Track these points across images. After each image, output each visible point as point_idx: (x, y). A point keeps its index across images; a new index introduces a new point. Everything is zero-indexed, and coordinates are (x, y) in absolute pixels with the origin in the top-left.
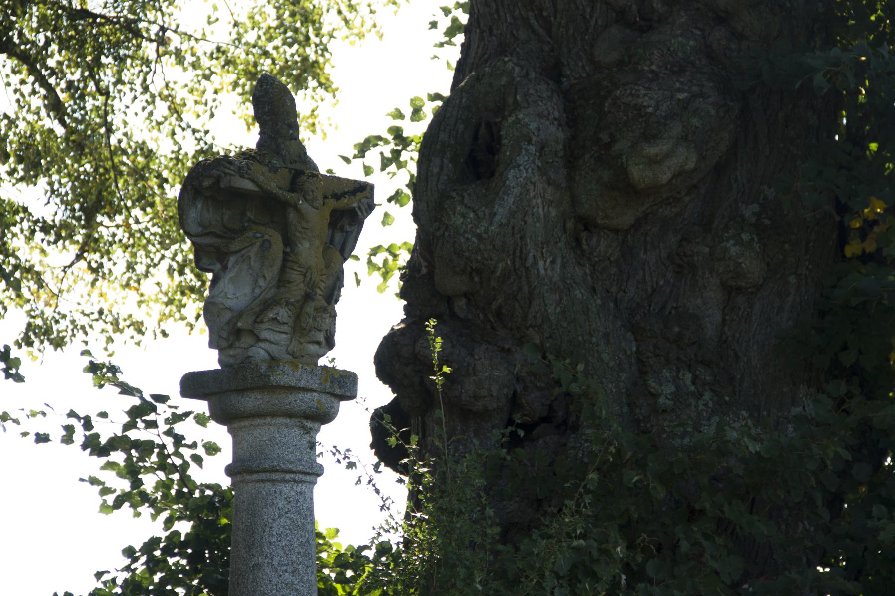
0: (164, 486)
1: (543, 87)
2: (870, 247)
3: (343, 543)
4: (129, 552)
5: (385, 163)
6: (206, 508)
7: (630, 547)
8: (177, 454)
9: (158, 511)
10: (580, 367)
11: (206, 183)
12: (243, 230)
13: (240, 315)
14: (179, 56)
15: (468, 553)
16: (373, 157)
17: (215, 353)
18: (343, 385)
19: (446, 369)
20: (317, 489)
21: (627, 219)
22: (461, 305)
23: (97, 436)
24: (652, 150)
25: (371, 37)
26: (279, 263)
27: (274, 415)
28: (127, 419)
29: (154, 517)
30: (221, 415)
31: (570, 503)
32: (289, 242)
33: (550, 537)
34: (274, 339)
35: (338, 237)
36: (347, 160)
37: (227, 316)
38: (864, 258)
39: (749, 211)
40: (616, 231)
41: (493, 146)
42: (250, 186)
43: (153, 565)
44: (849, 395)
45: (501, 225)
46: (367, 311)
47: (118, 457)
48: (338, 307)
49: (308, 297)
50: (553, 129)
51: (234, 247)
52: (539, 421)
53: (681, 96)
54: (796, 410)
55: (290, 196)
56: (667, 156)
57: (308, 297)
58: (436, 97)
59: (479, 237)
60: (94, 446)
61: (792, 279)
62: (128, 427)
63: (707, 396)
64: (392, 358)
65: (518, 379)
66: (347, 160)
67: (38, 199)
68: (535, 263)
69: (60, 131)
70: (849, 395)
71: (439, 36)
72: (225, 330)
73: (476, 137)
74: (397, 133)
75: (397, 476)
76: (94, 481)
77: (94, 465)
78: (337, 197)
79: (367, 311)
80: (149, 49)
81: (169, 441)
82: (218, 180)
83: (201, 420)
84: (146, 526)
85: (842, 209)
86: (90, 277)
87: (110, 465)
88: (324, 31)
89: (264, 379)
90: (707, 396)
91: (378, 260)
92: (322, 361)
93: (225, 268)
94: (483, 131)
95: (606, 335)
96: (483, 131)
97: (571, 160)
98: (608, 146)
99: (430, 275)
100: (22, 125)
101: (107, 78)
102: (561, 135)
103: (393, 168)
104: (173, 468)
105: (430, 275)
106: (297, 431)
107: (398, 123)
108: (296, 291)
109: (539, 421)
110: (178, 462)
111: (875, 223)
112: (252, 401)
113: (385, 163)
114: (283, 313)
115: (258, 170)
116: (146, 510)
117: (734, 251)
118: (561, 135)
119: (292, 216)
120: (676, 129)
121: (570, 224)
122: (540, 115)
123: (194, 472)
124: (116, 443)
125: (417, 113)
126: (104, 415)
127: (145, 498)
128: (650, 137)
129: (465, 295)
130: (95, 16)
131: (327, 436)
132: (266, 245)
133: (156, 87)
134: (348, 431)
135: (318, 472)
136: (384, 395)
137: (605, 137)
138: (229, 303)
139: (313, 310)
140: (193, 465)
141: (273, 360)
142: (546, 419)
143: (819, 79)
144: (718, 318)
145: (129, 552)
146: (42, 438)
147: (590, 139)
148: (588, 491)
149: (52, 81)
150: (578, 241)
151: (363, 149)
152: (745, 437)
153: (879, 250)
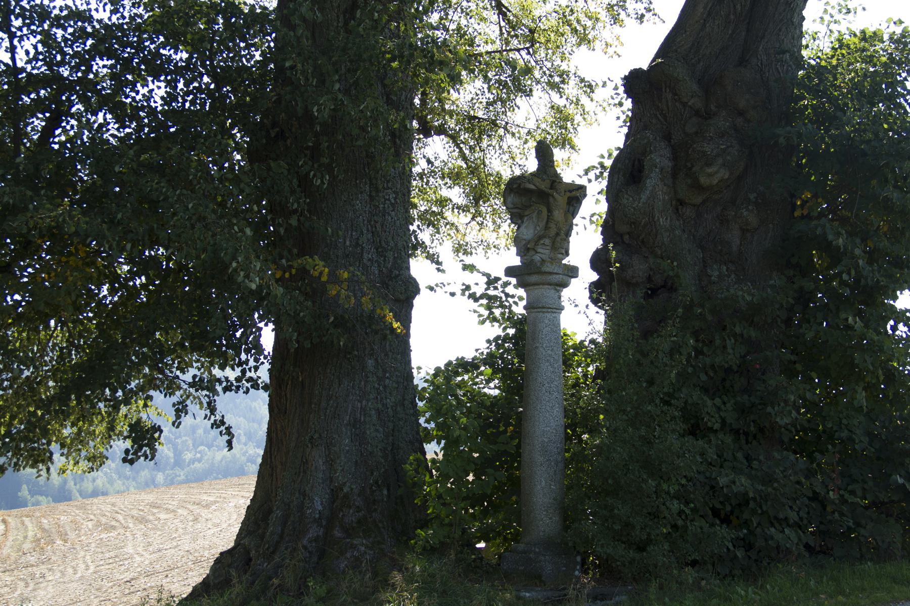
0: (503, 314)
1: (662, 144)
2: (805, 212)
3: (578, 339)
4: (488, 341)
5: (597, 178)
6: (519, 324)
7: (697, 341)
8: (507, 301)
9: (501, 325)
10: (675, 264)
11: (515, 186)
12: (531, 206)
13: (529, 242)
14: (513, 134)
15: (626, 343)
16: (592, 175)
17: (519, 258)
18: (573, 272)
19: (617, 265)
20: (561, 315)
21: (698, 200)
22: (626, 237)
23: (475, 293)
24: (710, 170)
25: (595, 125)
26: (545, 221)
27: (543, 284)
28: (486, 286)
29: (499, 327)
30: (519, 285)
31: (671, 322)
32: (550, 211)
33: (662, 336)
34: (543, 252)
35: (571, 208)
36: (580, 176)
37: (524, 242)
38: (802, 217)
39: (752, 196)
40: (694, 206)
41: (641, 169)
42: (533, 187)
43: (498, 346)
44: (794, 276)
45: (644, 203)
46: (585, 240)
47: (484, 301)
48: (571, 239)
49: (558, 234)
50: (667, 162)
51: (526, 213)
52: (659, 288)
53: (723, 147)
54: (772, 282)
55: (550, 191)
56: (716, 173)
57: (558, 234)
58: (619, 149)
59: (634, 208)
60: (473, 297)
61: (771, 226)
62: (486, 289)
63: (733, 276)
64: (598, 261)
65: (651, 269)
66: (580, 176)
67: (456, 195)
68: (658, 219)
69: (465, 166)
70: (794, 276)
71: (620, 123)
72: (523, 247)
73: (633, 166)
74: (602, 165)
75: (597, 309)
76: (475, 311)
77: (475, 306)
78: (570, 191)
79: (585, 240)
80: (501, 131)
81: (503, 295)
82: (520, 185)
83: (516, 287)
84: (495, 331)
85: (793, 196)
86: (478, 228)
87: (481, 305)
88: (575, 122)
89: (540, 268)
90: (733, 276)
91: (594, 219)
92: (564, 262)
93: (523, 222)
94: (636, 163)
95: (689, 250)
96: (636, 163)
97: (674, 175)
98: (690, 169)
99: (613, 224)
100: (450, 165)
101: (484, 144)
102: (670, 164)
103: (600, 180)
104: (505, 307)
105: (613, 224)
106: (553, 291)
107: (602, 160)
108: (553, 232)
109: (659, 288)
110: (507, 304)
111: (807, 202)
112: (534, 278)
113: (597, 178)
114: (547, 241)
115: (537, 181)
116: (496, 324)
117: (745, 213)
118: (670, 164)
119: (551, 199)
120: (720, 161)
121: (674, 203)
122: (661, 156)
123: (514, 308)
124: (482, 297)
125: (610, 155)
126: (477, 284)
127: (495, 319)
128: (709, 165)
129: (628, 233)
130: (479, 119)
131: (566, 293)
132: (540, 213)
133: (505, 147)
134: (577, 292)
135: (562, 308)
136: (594, 277)
137: (689, 165)
138: (525, 237)
139: (559, 240)
140: (514, 305)
141: (543, 261)
142: (664, 286)
143: (781, 140)
144: (739, 242)
145: (488, 341)
146: (453, 294)
147: (683, 165)
148: (678, 317)
149: (462, 145)
150: (677, 210)
151: (587, 172)
152: (745, 294)
153: (809, 213)
